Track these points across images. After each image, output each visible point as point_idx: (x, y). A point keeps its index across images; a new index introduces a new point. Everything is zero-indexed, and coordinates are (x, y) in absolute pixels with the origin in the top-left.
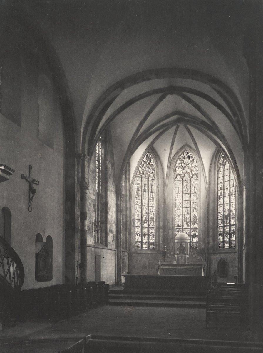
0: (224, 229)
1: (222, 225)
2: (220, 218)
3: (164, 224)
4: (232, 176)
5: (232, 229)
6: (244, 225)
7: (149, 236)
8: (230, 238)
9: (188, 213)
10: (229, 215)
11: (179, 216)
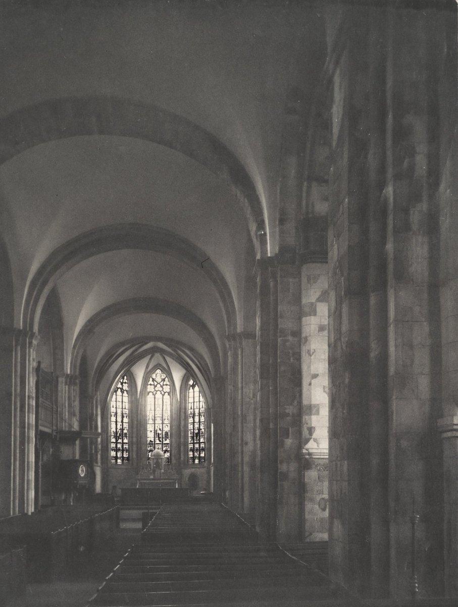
0: (194, 446)
2: (190, 435)
4: (201, 397)
5: (201, 446)
6: (212, 447)
7: (123, 451)
8: (200, 454)
10: (199, 433)
11: (151, 431)
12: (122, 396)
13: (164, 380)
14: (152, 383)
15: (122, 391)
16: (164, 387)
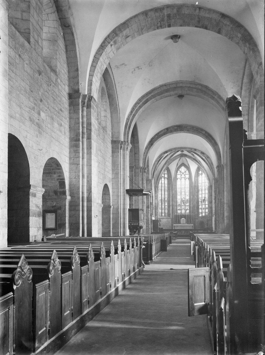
9: (184, 198)
12: (185, 181)
13: (185, 172)
14: (180, 173)
15: (165, 178)
16: (186, 175)
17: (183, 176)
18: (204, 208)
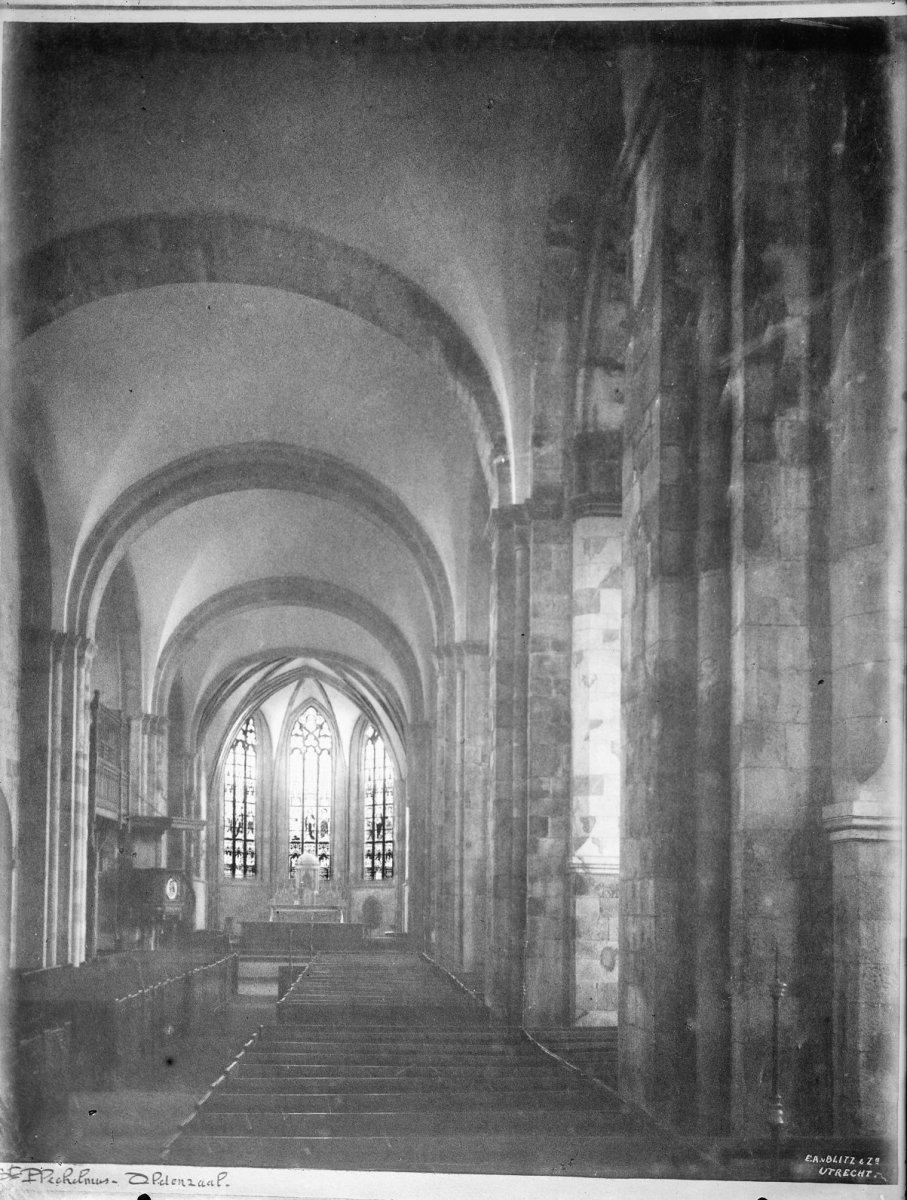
1: (371, 840)
3: (272, 834)
6: (407, 850)
8: (384, 862)
9: (313, 817)
16: (321, 739)
17: (311, 740)
18: (379, 854)
